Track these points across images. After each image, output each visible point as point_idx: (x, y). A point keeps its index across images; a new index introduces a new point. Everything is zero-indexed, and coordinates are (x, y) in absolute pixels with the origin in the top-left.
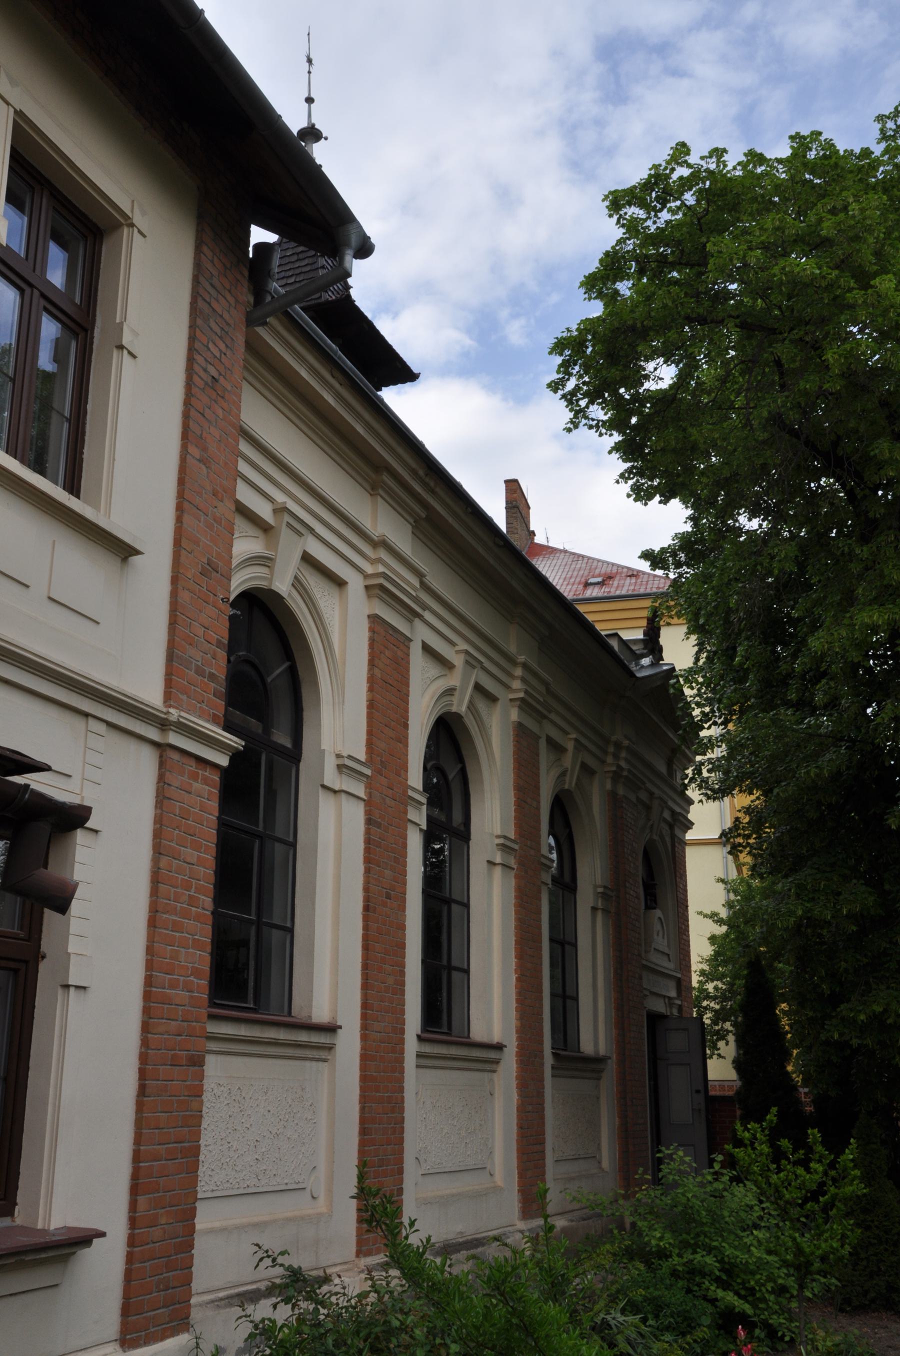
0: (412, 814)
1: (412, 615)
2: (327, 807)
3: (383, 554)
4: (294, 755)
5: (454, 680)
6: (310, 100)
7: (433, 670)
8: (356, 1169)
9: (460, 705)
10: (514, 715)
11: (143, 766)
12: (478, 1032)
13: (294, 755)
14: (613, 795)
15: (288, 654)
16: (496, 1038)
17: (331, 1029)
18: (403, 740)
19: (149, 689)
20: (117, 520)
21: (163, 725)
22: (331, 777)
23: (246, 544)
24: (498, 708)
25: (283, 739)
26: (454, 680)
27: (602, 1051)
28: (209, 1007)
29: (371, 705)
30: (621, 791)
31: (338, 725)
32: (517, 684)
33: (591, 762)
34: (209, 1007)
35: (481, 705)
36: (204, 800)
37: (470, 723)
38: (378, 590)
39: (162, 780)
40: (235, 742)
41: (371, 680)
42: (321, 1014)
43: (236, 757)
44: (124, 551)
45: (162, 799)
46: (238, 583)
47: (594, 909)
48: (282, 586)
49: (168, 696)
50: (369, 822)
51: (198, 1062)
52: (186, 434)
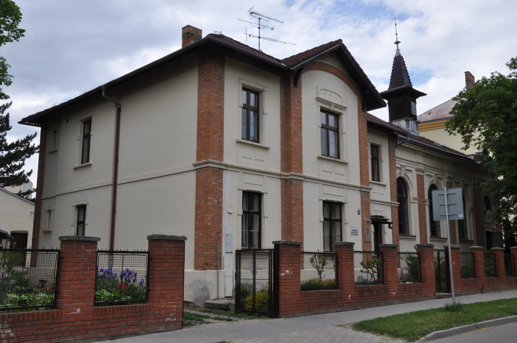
0: (426, 203)
1: (423, 172)
2: (412, 205)
3: (418, 164)
4: (406, 198)
5: (433, 178)
6: (396, 34)
7: (429, 178)
8: (19, 6)
9: (434, 182)
10: (446, 180)
11: (390, 208)
12: (442, 236)
13: (407, 198)
14: (474, 189)
15: (404, 183)
16: (446, 237)
17: (415, 236)
18: (424, 192)
19: (389, 200)
20: (384, 183)
21: (391, 204)
22: (412, 201)
23: (398, 171)
24: (443, 181)
25: (405, 196)
26: (433, 178)
27: (473, 239)
28: (341, 114)
29: (418, 188)
30: (476, 187)
31: (413, 192)
32: (447, 175)
33: (467, 183)
34: (341, 114)
35: (439, 181)
36: (396, 211)
37: (438, 185)
38: (418, 170)
39: (392, 210)
40: (399, 203)
41: (418, 184)
42: (413, 234)
43: (399, 205)
44: (385, 186)
45: (392, 212)
46: (397, 177)
47: (470, 212)
48: (403, 175)
49: (391, 200)
50: (419, 206)
51: (398, 240)
52: (390, 168)
